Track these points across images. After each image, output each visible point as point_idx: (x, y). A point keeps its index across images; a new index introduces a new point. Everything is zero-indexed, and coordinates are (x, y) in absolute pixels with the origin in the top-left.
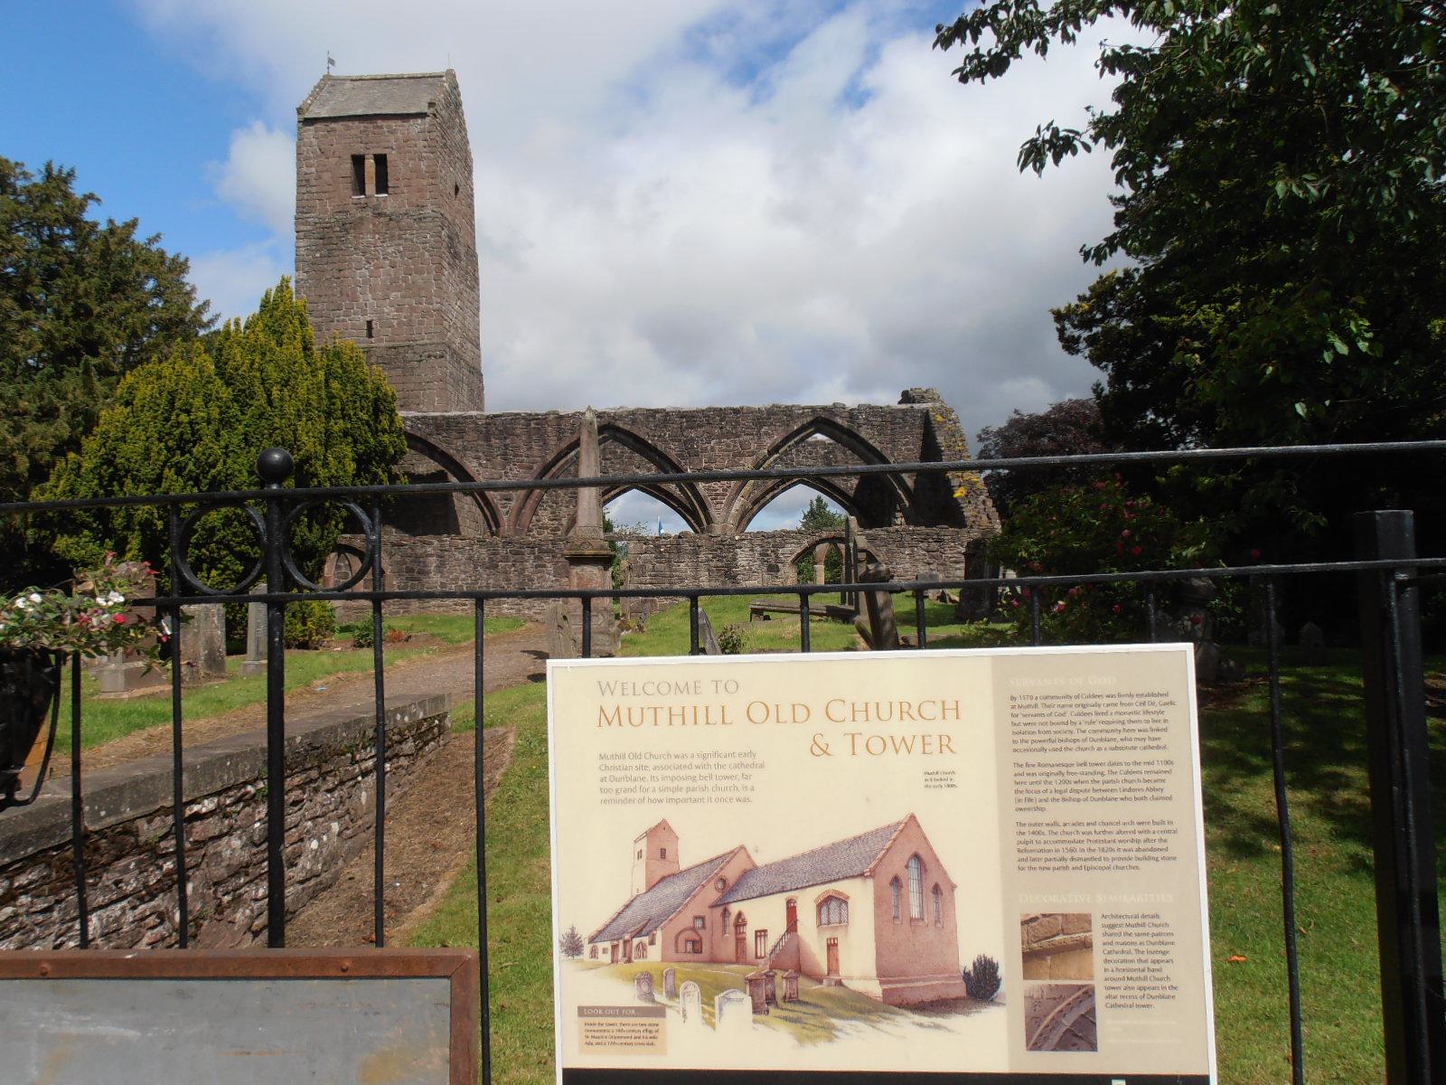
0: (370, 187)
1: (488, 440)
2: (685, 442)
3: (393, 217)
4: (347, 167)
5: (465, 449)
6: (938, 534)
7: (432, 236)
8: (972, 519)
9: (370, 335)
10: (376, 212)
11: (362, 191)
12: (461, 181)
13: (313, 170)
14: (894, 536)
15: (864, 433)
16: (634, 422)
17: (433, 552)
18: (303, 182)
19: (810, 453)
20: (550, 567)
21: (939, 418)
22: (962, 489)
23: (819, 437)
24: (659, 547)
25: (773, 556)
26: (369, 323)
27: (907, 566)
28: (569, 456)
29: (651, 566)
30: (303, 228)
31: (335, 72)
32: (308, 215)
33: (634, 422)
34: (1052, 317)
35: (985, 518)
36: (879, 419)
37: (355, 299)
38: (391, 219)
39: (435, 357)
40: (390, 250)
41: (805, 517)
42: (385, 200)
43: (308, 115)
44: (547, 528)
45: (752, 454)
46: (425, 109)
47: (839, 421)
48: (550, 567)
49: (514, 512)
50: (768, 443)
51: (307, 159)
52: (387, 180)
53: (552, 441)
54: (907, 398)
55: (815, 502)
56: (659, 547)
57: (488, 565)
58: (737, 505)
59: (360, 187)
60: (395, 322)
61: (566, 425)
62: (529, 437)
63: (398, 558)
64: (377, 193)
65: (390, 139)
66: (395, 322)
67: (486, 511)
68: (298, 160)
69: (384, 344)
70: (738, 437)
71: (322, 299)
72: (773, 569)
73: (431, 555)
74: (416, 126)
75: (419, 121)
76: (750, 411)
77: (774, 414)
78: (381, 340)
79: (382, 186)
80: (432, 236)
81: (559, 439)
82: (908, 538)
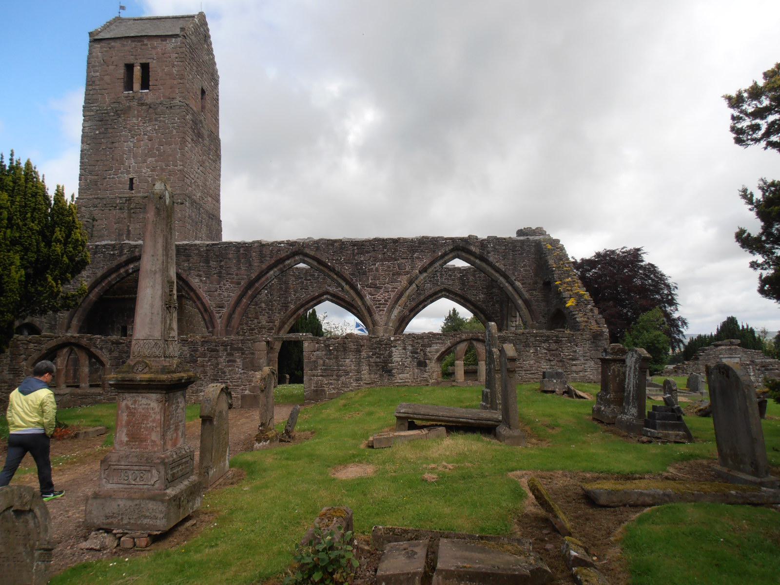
0: (137, 86)
1: (207, 261)
2: (357, 264)
3: (152, 106)
4: (121, 72)
5: (190, 269)
6: (557, 336)
7: (178, 119)
8: (584, 324)
9: (131, 188)
10: (140, 102)
11: (132, 89)
12: (206, 85)
13: (98, 74)
14: (521, 337)
15: (492, 258)
16: (318, 249)
19: (450, 276)
20: (239, 362)
21: (549, 247)
22: (572, 300)
24: (329, 346)
25: (422, 353)
26: (131, 180)
27: (532, 362)
28: (268, 275)
29: (321, 362)
30: (88, 113)
31: (124, 15)
32: (92, 105)
33: (318, 249)
34: (725, 103)
35: (593, 323)
36: (504, 248)
38: (150, 107)
39: (177, 203)
40: (149, 129)
41: (446, 319)
42: (147, 94)
43: (96, 37)
44: (265, 328)
45: (408, 273)
46: (178, 32)
47: (473, 248)
48: (239, 362)
49: (226, 317)
50: (419, 265)
51: (94, 66)
52: (149, 81)
53: (256, 264)
55: (452, 312)
56: (329, 346)
57: (189, 360)
58: (395, 312)
59: (129, 86)
60: (150, 179)
61: (266, 251)
62: (239, 261)
63: (116, 354)
64: (142, 89)
65: (151, 54)
66: (150, 179)
68: (88, 67)
69: (141, 195)
70: (396, 260)
71: (99, 163)
72: (422, 364)
74: (171, 44)
75: (173, 40)
76: (405, 240)
77: (424, 243)
78: (139, 192)
79: (145, 85)
80: (178, 119)
81: (262, 262)
82: (532, 339)
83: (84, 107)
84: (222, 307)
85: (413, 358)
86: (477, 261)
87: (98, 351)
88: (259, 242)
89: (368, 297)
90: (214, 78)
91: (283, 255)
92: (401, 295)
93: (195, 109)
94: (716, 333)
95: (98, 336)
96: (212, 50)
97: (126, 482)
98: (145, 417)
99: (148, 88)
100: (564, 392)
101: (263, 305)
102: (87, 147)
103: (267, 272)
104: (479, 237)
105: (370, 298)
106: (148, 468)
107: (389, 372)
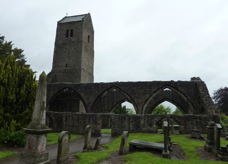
0: (69, 36)
4: (65, 32)
9: (66, 66)
12: (89, 34)
17: (64, 116)
47: (172, 85)
73: (64, 117)
83: (55, 43)
84: (90, 103)
85: (147, 123)
86: (174, 89)
87: (52, 116)
88: (101, 83)
89: (136, 101)
90: (92, 32)
91: (109, 87)
92: (147, 100)
93: (86, 42)
94: (48, 70)
95: (52, 112)
96: (92, 24)
97: (26, 161)
98: (33, 142)
99: (72, 37)
100: (200, 138)
101: (106, 102)
102: (55, 54)
103: (104, 93)
104: (174, 81)
105: (137, 102)
106: (31, 157)
107: (139, 127)
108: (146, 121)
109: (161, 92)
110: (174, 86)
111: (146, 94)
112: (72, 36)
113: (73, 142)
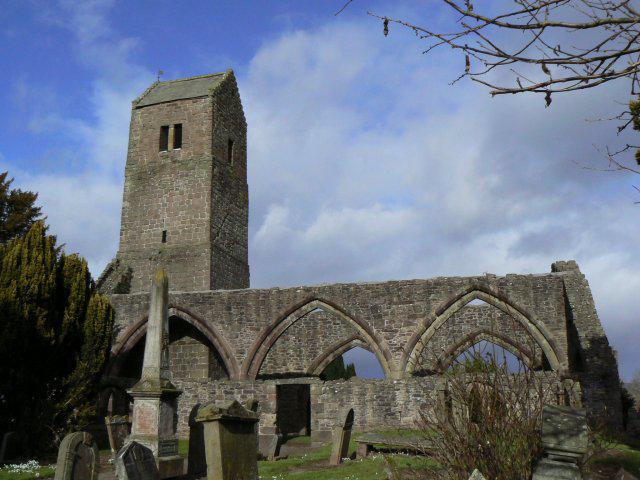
0: (170, 145)
1: (229, 309)
4: (158, 133)
9: (164, 240)
18: (132, 145)
23: (477, 303)
26: (164, 232)
37: (156, 216)
50: (436, 306)
54: (554, 268)
59: (163, 146)
67: (574, 455)
91: (299, 301)
101: (291, 352)
108: (411, 398)
109: (449, 464)
110: (496, 292)
111: (414, 317)
112: (178, 144)
113: (572, 299)
